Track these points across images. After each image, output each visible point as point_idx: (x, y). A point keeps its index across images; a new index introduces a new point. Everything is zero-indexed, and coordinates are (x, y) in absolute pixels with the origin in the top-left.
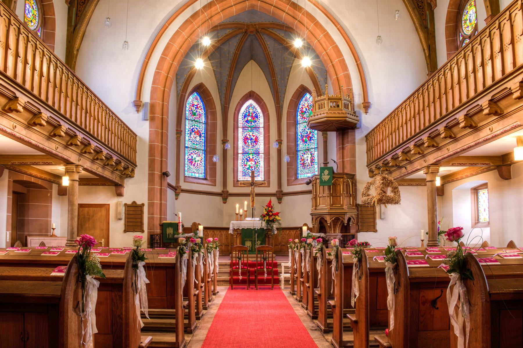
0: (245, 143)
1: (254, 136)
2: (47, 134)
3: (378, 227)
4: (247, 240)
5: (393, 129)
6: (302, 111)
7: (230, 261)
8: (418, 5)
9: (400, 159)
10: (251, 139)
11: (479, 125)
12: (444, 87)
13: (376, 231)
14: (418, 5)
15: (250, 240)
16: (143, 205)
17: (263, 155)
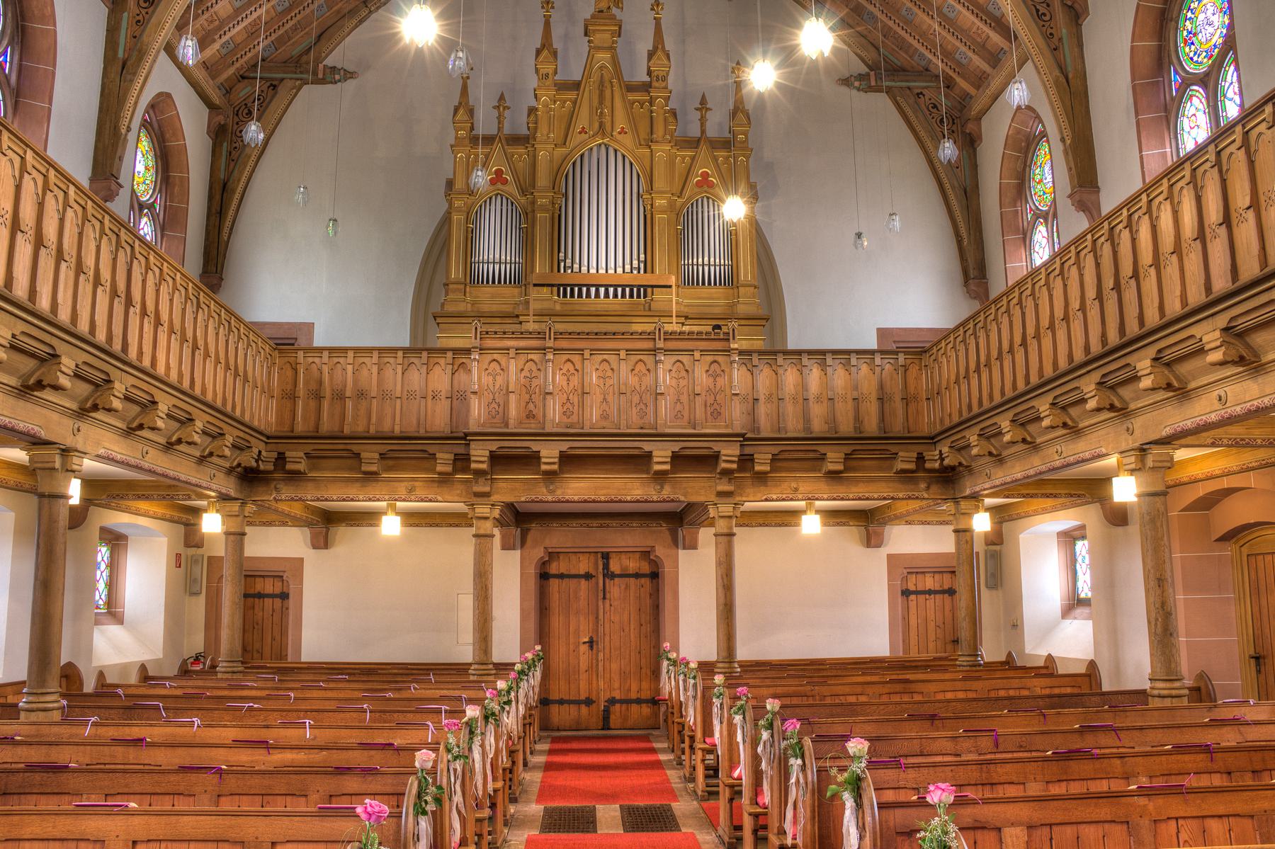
2: (74, 406)
5: (983, 359)
7: (738, 452)
8: (1038, 11)
9: (1007, 438)
11: (1132, 406)
12: (1150, 248)
14: (1038, 11)
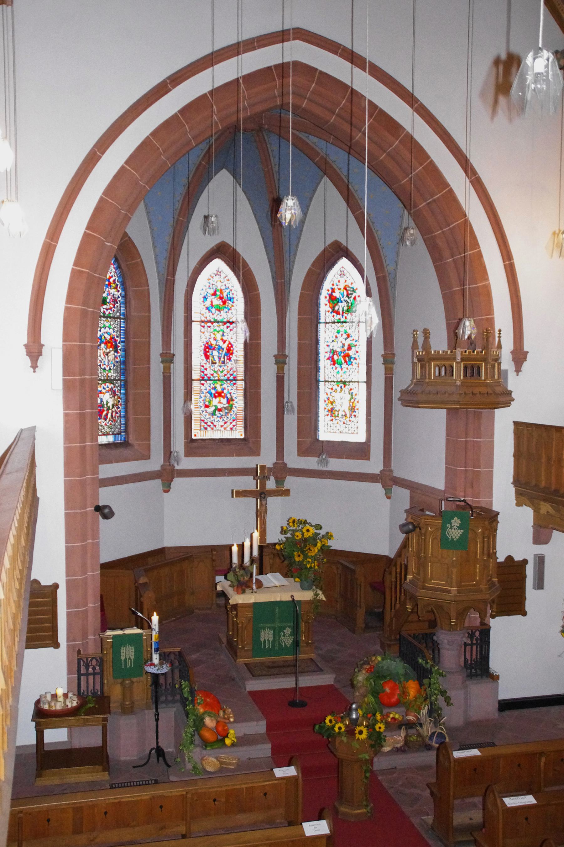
0: (207, 357)
1: (224, 342)
3: (529, 606)
4: (264, 628)
6: (332, 298)
10: (220, 348)
13: (524, 614)
15: (270, 628)
16: (56, 586)
17: (243, 383)
